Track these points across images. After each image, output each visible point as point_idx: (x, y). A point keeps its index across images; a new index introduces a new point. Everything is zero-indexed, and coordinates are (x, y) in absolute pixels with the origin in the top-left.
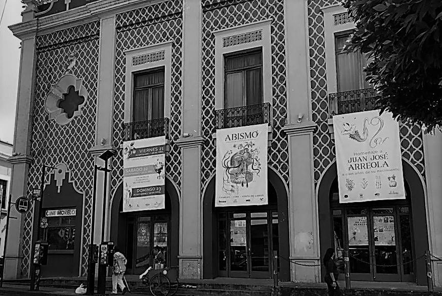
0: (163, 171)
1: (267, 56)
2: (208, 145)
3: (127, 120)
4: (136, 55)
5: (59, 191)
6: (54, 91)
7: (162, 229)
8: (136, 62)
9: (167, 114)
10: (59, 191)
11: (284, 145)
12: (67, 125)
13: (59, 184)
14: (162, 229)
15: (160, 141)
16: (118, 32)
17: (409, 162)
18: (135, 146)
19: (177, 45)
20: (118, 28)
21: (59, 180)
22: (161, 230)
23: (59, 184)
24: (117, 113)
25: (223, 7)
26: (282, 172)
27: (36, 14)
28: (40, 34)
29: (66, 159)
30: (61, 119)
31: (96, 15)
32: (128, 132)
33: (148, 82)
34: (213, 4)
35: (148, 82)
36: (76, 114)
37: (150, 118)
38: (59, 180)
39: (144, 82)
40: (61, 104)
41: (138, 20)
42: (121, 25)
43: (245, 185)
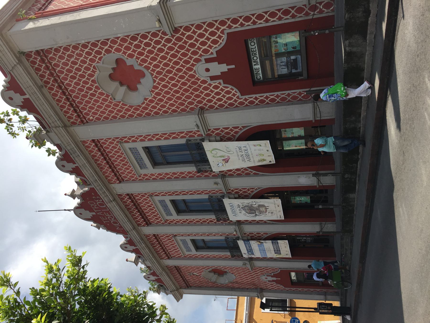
0: (261, 241)
1: (148, 144)
2: (224, 175)
3: (192, 169)
4: (184, 250)
5: (233, 66)
6: (119, 97)
7: (281, 64)
8: (142, 166)
9: (206, 197)
10: (233, 66)
11: (187, 29)
12: (152, 75)
13: (224, 68)
14: (281, 64)
15: (241, 244)
16: (87, 122)
17: (237, 136)
18: (246, 252)
19: (122, 140)
20: (169, 258)
21: (218, 69)
22: (284, 65)
23: (224, 68)
24: (209, 223)
25: (52, 67)
26: (219, 43)
27: (166, 289)
28: (179, 287)
29: (190, 69)
30: (146, 85)
31: (142, 239)
32: (203, 167)
33: (182, 207)
34: (52, 77)
35: (158, 156)
36: (137, 67)
37: (188, 152)
38: (218, 69)
39: (159, 158)
40: (133, 88)
41: (44, 68)
42: (72, 109)
43: (267, 208)
